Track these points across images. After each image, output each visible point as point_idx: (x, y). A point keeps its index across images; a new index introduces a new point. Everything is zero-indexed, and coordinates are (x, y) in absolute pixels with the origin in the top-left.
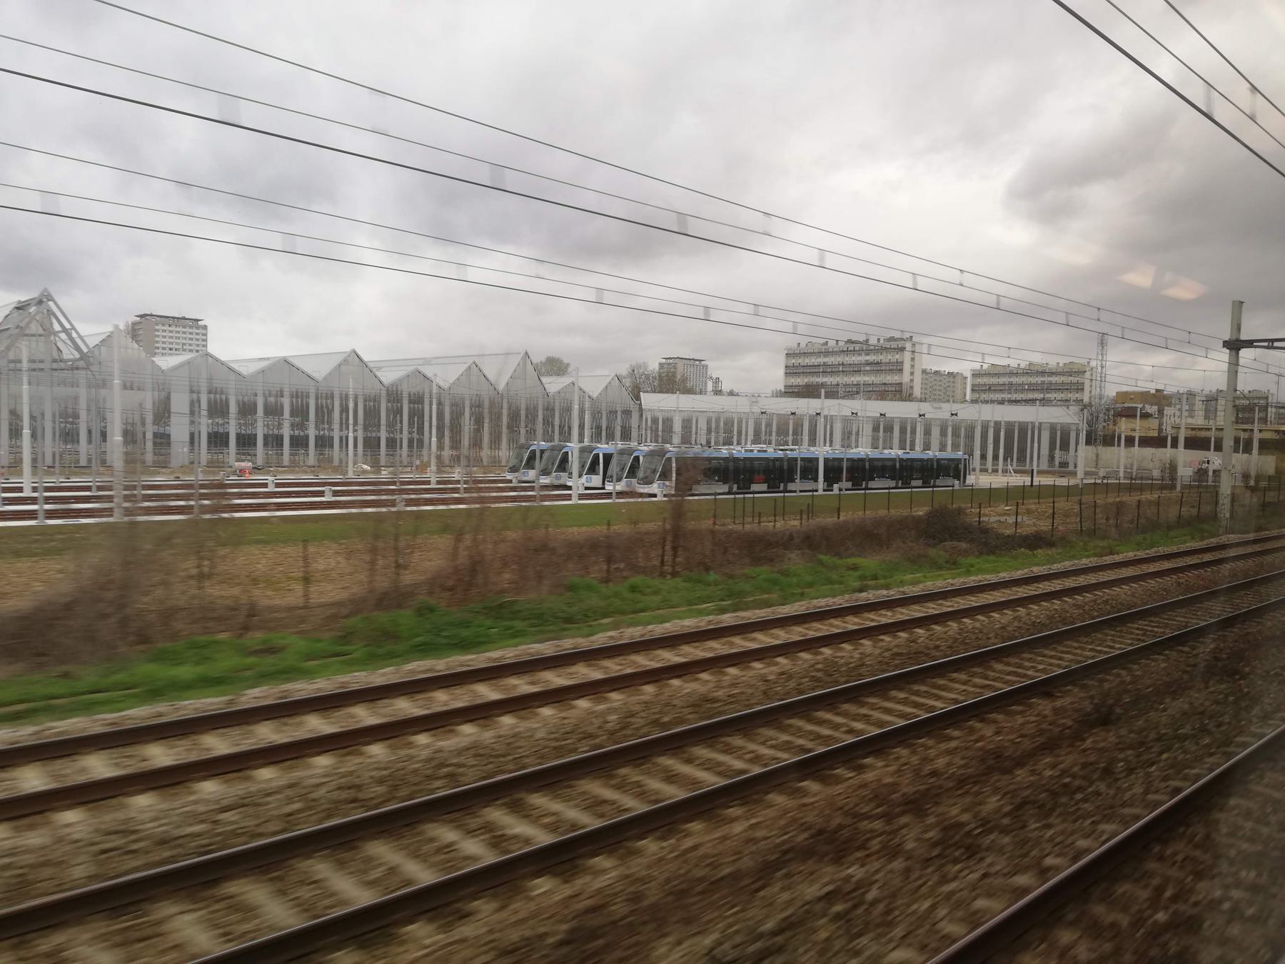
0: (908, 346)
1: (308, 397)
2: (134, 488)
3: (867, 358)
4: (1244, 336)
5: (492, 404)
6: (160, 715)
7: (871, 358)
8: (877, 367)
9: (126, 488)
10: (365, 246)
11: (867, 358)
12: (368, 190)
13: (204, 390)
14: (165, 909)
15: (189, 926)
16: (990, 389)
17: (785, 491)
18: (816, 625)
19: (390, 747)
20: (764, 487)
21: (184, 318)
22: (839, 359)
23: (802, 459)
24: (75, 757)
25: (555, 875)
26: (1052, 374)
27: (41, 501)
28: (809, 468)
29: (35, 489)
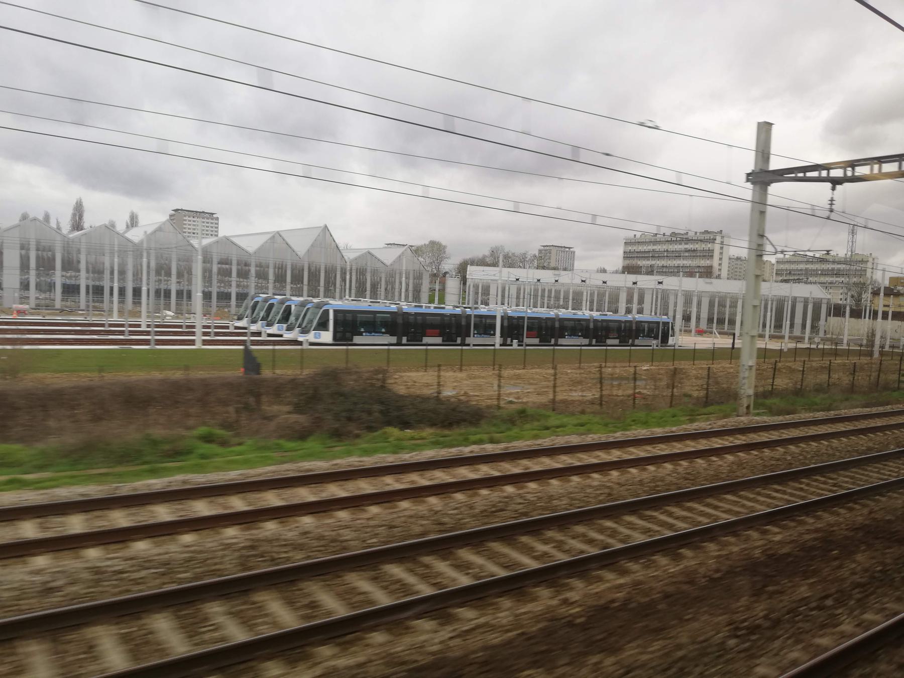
0: (871, 260)
1: (268, 267)
2: (209, 327)
3: (686, 246)
4: (775, 164)
5: (259, 265)
6: (672, 432)
7: (690, 246)
8: (693, 254)
9: (204, 327)
10: (356, 166)
11: (686, 246)
12: (359, 129)
13: (33, 247)
14: (261, 597)
15: (111, 648)
16: (644, 255)
17: (463, 344)
18: (662, 446)
19: (155, 543)
20: (616, 342)
21: (203, 212)
22: (665, 247)
23: (529, 318)
24: (16, 522)
25: (476, 607)
26: (839, 263)
27: (152, 333)
28: (485, 326)
29: (148, 326)
